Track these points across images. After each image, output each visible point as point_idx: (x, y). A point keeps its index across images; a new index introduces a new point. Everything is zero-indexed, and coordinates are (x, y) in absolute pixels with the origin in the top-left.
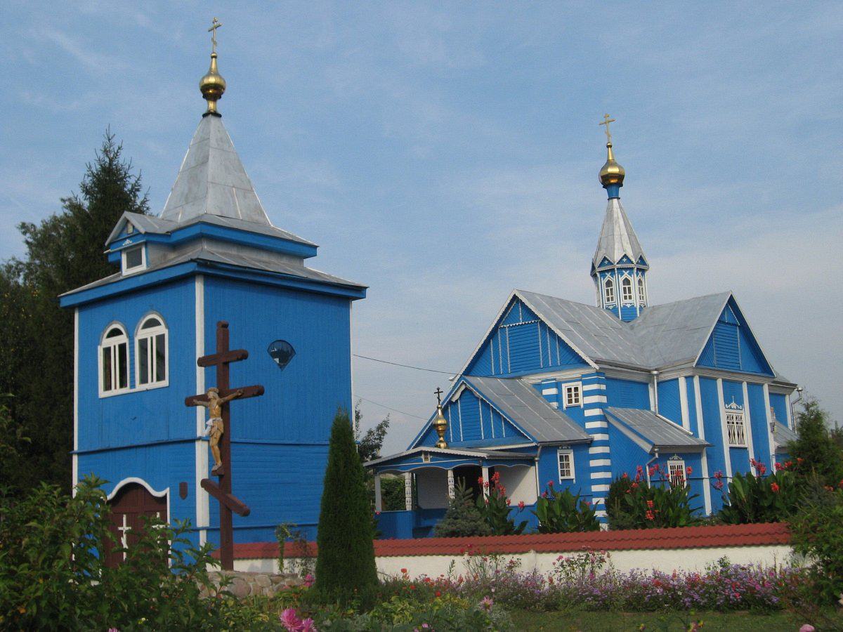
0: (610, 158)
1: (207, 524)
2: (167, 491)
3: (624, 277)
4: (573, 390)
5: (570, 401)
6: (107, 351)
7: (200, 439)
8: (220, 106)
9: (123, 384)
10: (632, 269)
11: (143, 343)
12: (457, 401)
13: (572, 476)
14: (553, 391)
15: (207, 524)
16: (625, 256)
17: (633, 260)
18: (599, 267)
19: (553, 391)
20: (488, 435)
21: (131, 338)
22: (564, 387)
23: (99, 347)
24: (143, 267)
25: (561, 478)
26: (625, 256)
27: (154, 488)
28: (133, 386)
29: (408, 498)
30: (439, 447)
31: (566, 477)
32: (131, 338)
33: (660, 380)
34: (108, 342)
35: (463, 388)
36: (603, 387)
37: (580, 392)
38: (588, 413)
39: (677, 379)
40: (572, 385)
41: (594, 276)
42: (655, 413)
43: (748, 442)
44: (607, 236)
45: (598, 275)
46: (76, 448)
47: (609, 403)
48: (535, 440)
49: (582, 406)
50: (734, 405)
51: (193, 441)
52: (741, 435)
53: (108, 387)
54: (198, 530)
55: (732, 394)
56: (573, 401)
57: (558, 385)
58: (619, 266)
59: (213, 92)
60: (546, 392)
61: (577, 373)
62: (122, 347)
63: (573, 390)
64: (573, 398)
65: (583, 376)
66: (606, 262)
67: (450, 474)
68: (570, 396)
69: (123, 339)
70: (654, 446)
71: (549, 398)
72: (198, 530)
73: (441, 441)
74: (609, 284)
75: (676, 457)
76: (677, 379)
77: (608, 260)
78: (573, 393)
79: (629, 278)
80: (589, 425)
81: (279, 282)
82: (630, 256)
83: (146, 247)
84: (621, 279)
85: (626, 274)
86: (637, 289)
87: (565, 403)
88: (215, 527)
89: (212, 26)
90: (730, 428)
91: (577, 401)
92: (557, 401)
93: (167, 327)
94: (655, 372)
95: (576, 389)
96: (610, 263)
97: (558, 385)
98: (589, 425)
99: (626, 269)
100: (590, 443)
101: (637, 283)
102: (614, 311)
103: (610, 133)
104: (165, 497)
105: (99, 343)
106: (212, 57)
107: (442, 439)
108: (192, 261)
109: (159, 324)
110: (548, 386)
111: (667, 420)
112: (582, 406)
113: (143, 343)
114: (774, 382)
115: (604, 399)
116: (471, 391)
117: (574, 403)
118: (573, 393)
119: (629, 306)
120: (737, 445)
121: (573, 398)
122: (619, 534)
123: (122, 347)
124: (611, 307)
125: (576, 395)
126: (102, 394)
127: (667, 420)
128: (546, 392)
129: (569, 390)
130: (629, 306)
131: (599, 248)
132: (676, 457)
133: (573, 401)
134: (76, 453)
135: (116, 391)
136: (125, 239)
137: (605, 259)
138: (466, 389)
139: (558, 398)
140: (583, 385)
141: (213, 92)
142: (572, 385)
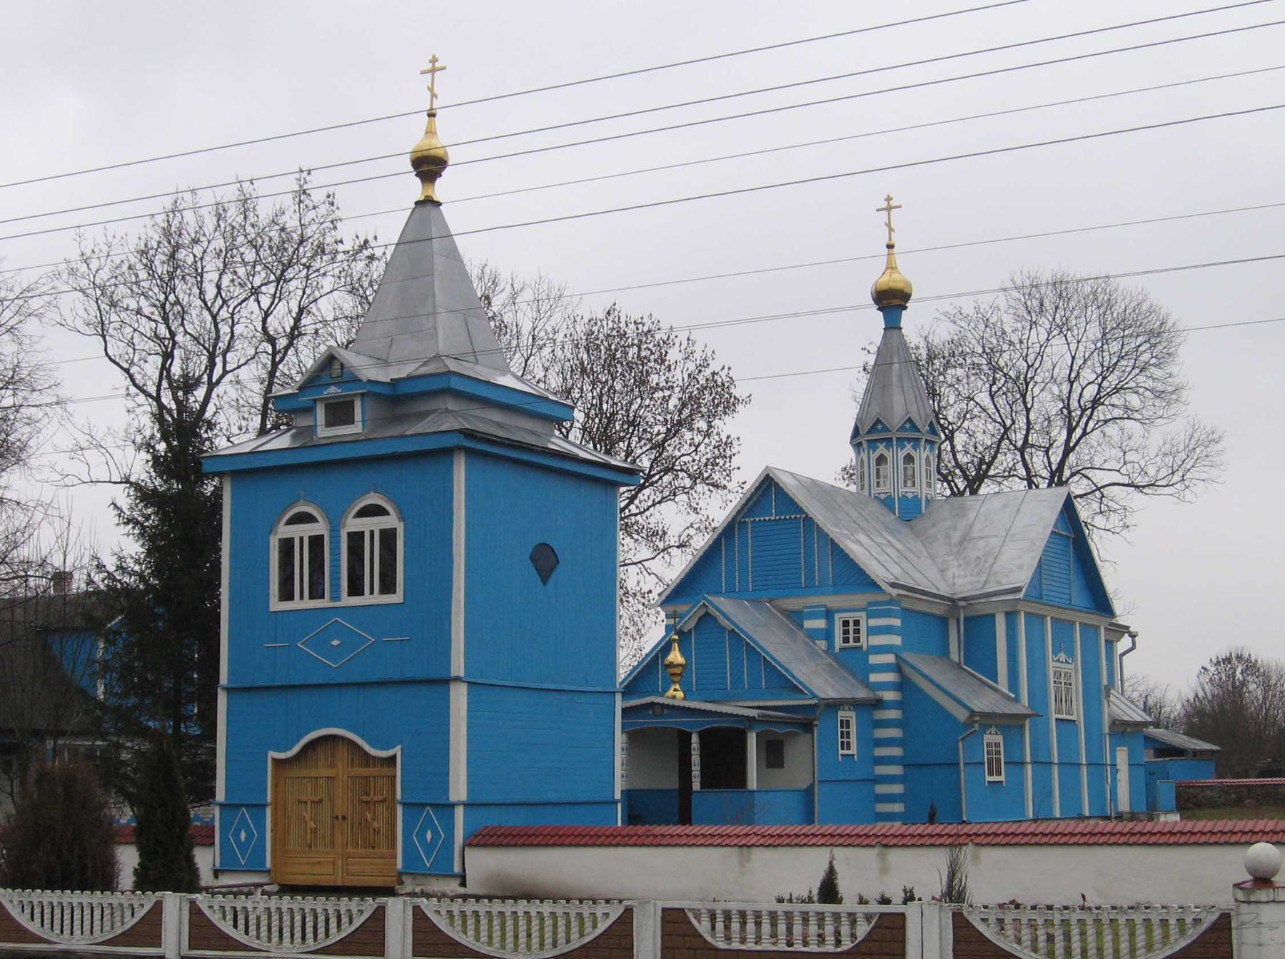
1: (463, 796)
2: (397, 751)
3: (905, 452)
4: (851, 624)
5: (846, 640)
6: (287, 547)
7: (458, 679)
8: (442, 188)
10: (918, 440)
11: (356, 540)
12: (690, 631)
13: (853, 751)
14: (821, 624)
15: (463, 796)
18: (869, 432)
19: (821, 624)
20: (737, 683)
21: (335, 529)
22: (838, 619)
23: (271, 537)
24: (356, 429)
25: (841, 752)
26: (910, 420)
27: (373, 746)
28: (336, 597)
31: (846, 752)
32: (335, 529)
33: (969, 615)
34: (284, 531)
35: (702, 612)
36: (897, 622)
37: (863, 627)
38: (874, 659)
39: (993, 615)
40: (850, 616)
42: (959, 664)
43: (1078, 714)
46: (224, 678)
47: (907, 645)
48: (815, 696)
49: (865, 647)
50: (1062, 656)
52: (1069, 702)
53: (287, 594)
54: (453, 806)
55: (1064, 644)
56: (851, 640)
57: (829, 614)
58: (900, 435)
60: (809, 624)
61: (859, 599)
62: (317, 542)
63: (851, 624)
64: (851, 635)
65: (870, 604)
66: (880, 427)
67: (695, 739)
68: (846, 632)
69: (320, 528)
70: (973, 713)
71: (813, 635)
72: (453, 806)
75: (993, 730)
78: (851, 628)
79: (913, 453)
80: (873, 678)
81: (526, 457)
83: (362, 400)
84: (902, 454)
85: (908, 448)
87: (838, 642)
90: (1057, 690)
91: (857, 640)
92: (827, 639)
93: (402, 518)
94: (962, 603)
95: (857, 623)
96: (885, 429)
97: (829, 614)
98: (873, 678)
99: (909, 440)
100: (878, 704)
102: (887, 503)
104: (394, 757)
105: (271, 529)
109: (387, 513)
110: (814, 616)
111: (696, 758)
112: (865, 647)
113: (356, 540)
114: (1112, 624)
115: (896, 640)
117: (851, 643)
118: (851, 628)
119: (910, 496)
121: (851, 635)
122: (631, 829)
124: (883, 497)
125: (857, 631)
126: (276, 605)
128: (809, 624)
129: (846, 623)
130: (910, 496)
132: (993, 730)
134: (224, 688)
135: (301, 603)
136: (328, 385)
137: (878, 421)
138: (707, 614)
139: (828, 634)
140: (868, 618)
142: (846, 616)
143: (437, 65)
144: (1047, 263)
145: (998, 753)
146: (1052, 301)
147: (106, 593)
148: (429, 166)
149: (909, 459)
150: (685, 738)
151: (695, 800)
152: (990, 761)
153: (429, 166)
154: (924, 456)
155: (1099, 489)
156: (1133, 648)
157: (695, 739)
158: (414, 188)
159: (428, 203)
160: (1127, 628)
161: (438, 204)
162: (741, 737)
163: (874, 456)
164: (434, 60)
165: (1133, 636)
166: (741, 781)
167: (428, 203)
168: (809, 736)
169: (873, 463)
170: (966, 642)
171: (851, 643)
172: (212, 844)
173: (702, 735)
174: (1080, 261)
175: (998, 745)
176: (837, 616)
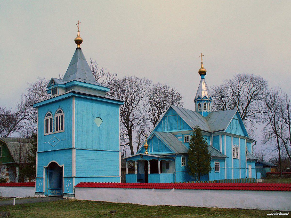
0: (203, 66)
4: (187, 137)
5: (186, 141)
8: (81, 46)
9: (51, 131)
11: (57, 118)
16: (205, 96)
17: (208, 97)
26: (205, 96)
28: (54, 132)
29: (136, 170)
30: (146, 153)
40: (187, 136)
41: (195, 102)
44: (200, 89)
45: (196, 102)
51: (71, 149)
56: (187, 141)
59: (202, 73)
63: (187, 137)
64: (187, 140)
67: (149, 162)
73: (146, 152)
74: (200, 105)
76: (219, 135)
77: (200, 97)
78: (187, 138)
82: (206, 96)
83: (58, 88)
86: (198, 107)
88: (68, 177)
89: (78, 23)
94: (213, 133)
95: (188, 137)
101: (208, 105)
103: (202, 59)
106: (78, 32)
107: (146, 151)
108: (72, 92)
111: (149, 167)
114: (248, 139)
116: (156, 136)
118: (187, 138)
119: (205, 112)
120: (236, 158)
121: (187, 140)
123: (51, 119)
124: (200, 112)
126: (45, 134)
127: (149, 167)
129: (186, 137)
131: (197, 94)
133: (187, 141)
137: (199, 97)
141: (202, 73)
143: (79, 22)
144: (242, 72)
145: (218, 165)
146: (243, 79)
147: (201, 141)
148: (78, 42)
149: (205, 104)
150: (146, 162)
151: (149, 176)
152: (216, 168)
153: (78, 42)
154: (208, 104)
155: (254, 114)
156: (255, 144)
157: (149, 162)
158: (76, 46)
159: (79, 49)
160: (254, 140)
161: (81, 49)
162: (157, 162)
163: (198, 104)
164: (202, 54)
165: (256, 142)
166: (158, 173)
167: (79, 49)
168: (224, 162)
169: (198, 105)
170: (213, 142)
171: (187, 141)
172: (35, 187)
173: (150, 161)
174: (249, 72)
175: (184, 164)
176: (184, 136)
